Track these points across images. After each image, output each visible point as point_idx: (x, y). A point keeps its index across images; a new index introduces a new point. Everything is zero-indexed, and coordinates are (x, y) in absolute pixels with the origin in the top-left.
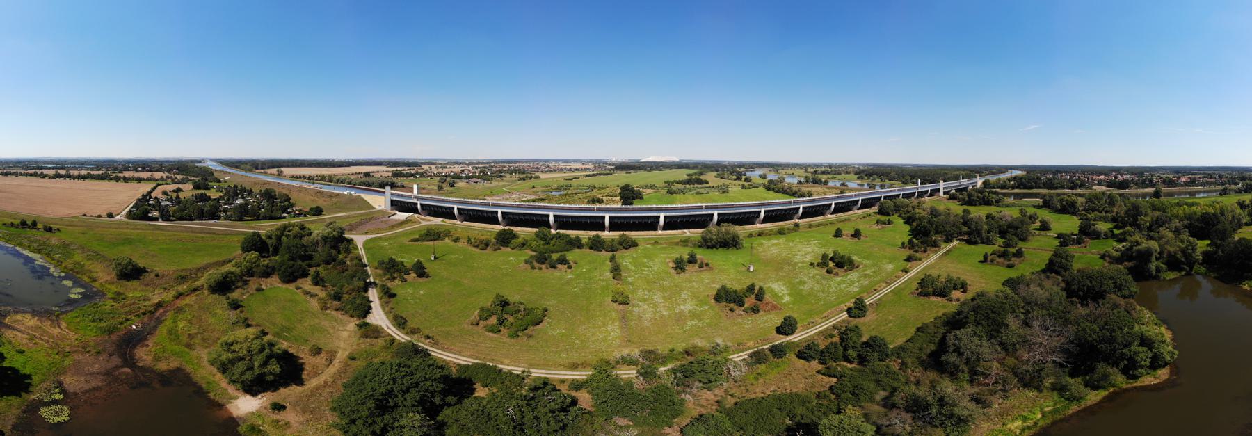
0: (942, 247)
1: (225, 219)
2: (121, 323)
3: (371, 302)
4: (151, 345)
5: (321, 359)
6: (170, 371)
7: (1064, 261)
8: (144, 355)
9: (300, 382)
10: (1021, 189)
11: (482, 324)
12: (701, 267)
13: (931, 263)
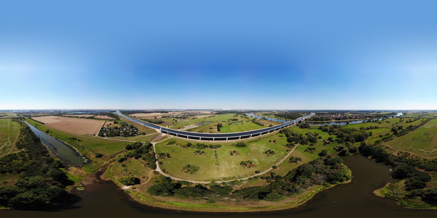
0: (295, 146)
1: (121, 136)
2: (97, 170)
3: (156, 165)
4: (104, 175)
5: (145, 179)
6: (108, 180)
7: (325, 153)
8: (102, 177)
9: (140, 184)
11: (183, 171)
12: (237, 154)
13: (294, 152)
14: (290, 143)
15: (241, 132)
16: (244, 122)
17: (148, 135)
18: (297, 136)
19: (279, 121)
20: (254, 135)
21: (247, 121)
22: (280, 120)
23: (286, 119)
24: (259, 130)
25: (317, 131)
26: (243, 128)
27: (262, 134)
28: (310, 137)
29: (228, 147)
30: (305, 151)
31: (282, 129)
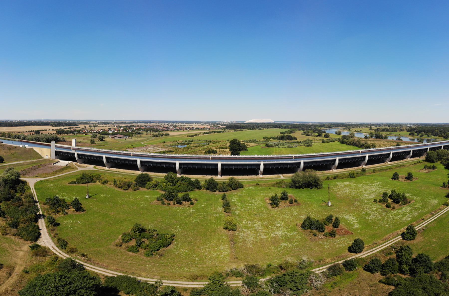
3: (40, 229)
16: (313, 143)
17: (9, 162)
29: (263, 189)
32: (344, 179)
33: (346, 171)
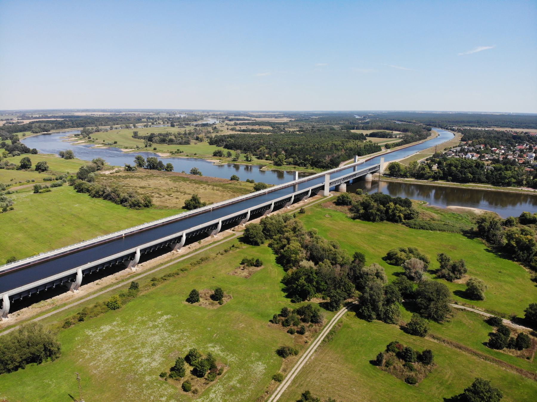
0: (325, 320)
10: (448, 181)
14: (298, 306)
15: (9, 262)
16: (14, 196)
18: (334, 261)
19: (242, 173)
20: (96, 267)
21: (37, 190)
22: (247, 168)
23: (276, 164)
24: (123, 233)
25: (454, 248)
26: (20, 235)
27: (147, 255)
28: (411, 278)
30: (376, 362)
31: (257, 221)
32: (99, 316)
33: (101, 289)
